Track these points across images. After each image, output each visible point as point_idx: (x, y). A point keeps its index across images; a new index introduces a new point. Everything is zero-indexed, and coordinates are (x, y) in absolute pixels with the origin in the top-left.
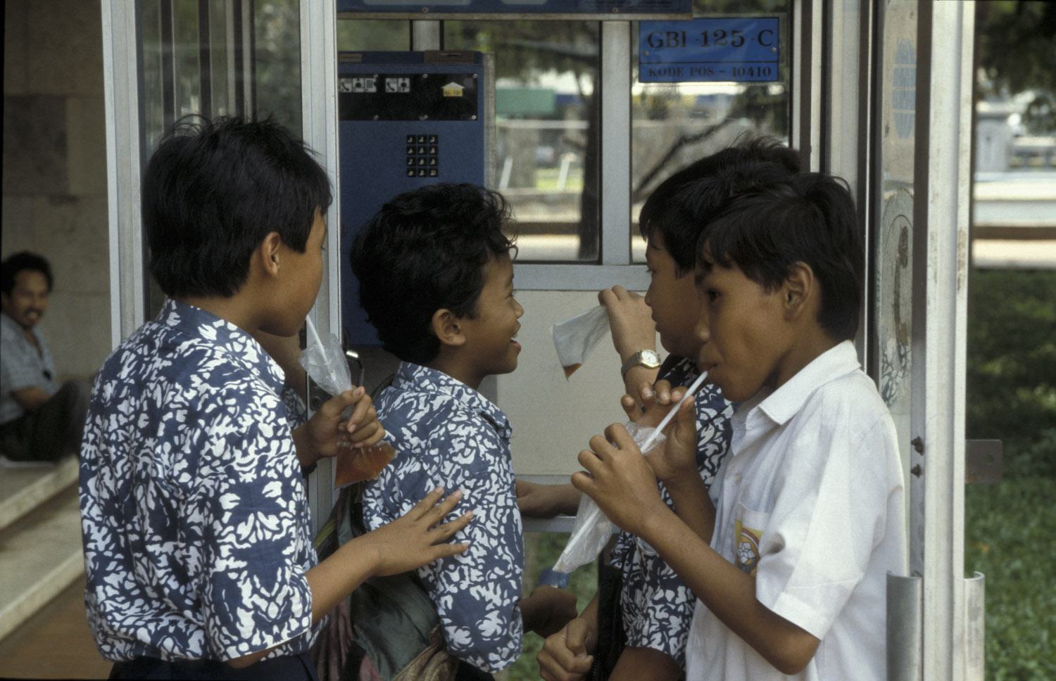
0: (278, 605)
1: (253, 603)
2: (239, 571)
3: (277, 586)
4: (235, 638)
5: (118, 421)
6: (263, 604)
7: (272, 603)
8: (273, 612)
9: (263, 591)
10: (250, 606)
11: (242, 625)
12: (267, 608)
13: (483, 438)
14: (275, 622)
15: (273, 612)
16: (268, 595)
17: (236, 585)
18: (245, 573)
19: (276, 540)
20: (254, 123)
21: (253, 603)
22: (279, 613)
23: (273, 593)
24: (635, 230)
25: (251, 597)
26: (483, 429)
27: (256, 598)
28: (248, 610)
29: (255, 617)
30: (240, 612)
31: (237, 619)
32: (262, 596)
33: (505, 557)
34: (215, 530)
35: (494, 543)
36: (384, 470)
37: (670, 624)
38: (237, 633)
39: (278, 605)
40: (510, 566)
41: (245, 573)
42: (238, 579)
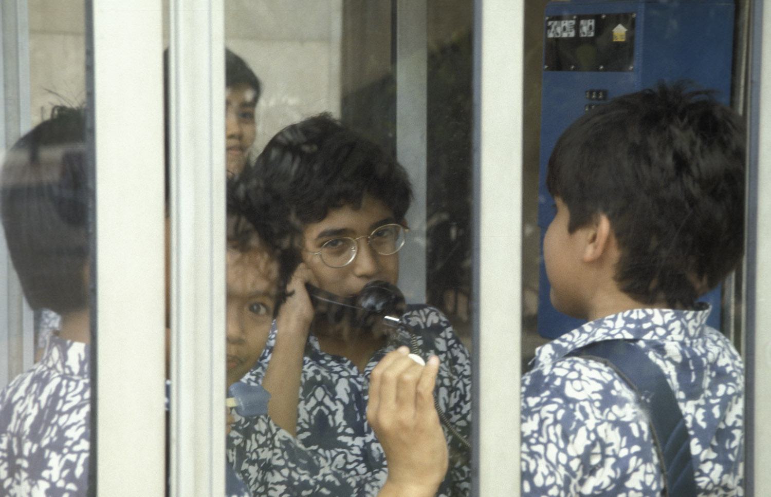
0: (315, 398)
1: (336, 404)
2: (344, 433)
3: (315, 412)
4: (352, 380)
5: (257, 441)
6: (327, 401)
7: (320, 400)
8: (319, 392)
9: (326, 412)
10: (338, 402)
11: (346, 389)
12: (324, 397)
13: (703, 407)
14: (320, 384)
15: (319, 392)
16: (323, 408)
17: (347, 423)
18: (340, 430)
19: (315, 445)
20: (306, 381)
21: (336, 404)
22: (315, 390)
23: (318, 408)
24: (582, 331)
25: (337, 410)
26: (708, 393)
27: (333, 408)
28: (340, 400)
29: (335, 394)
30: (346, 400)
31: (349, 395)
32: (328, 408)
33: (304, 478)
34: (6, 469)
35: (285, 472)
36: (648, 401)
37: (265, 459)
38: (351, 384)
39: (315, 398)
40: (312, 482)
41: (340, 430)
42: (346, 427)
